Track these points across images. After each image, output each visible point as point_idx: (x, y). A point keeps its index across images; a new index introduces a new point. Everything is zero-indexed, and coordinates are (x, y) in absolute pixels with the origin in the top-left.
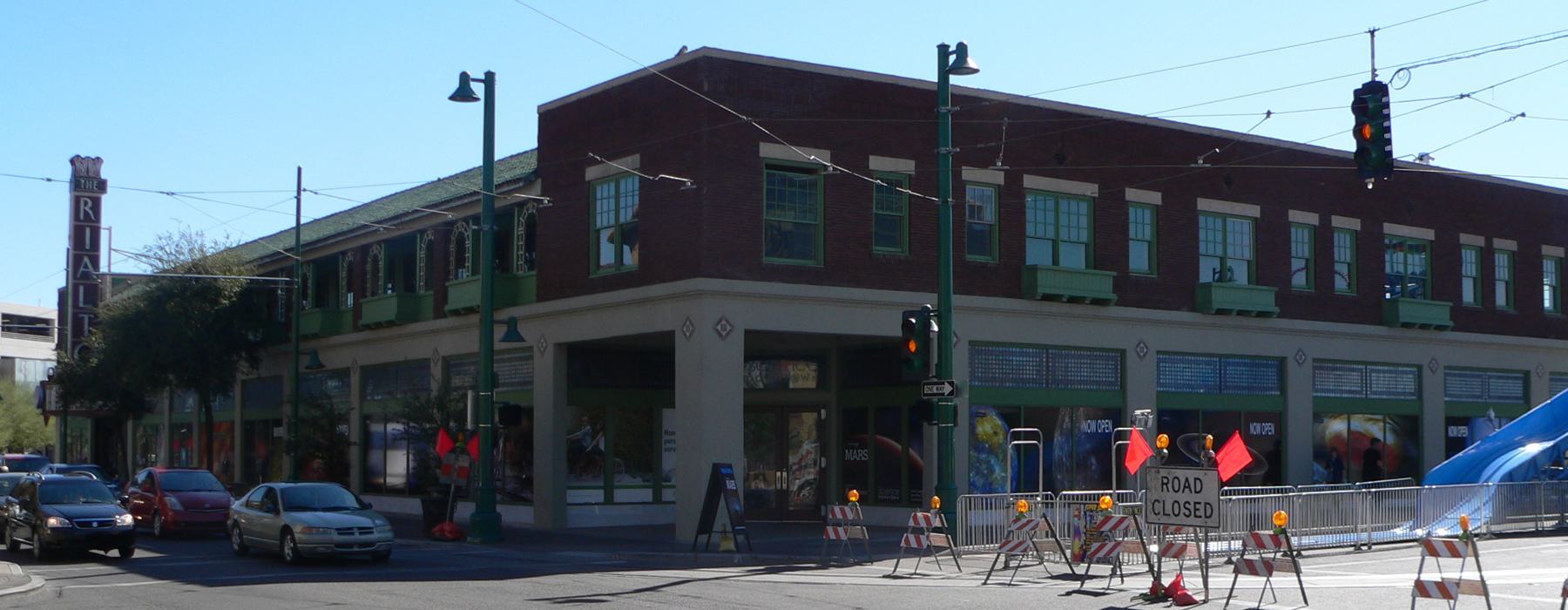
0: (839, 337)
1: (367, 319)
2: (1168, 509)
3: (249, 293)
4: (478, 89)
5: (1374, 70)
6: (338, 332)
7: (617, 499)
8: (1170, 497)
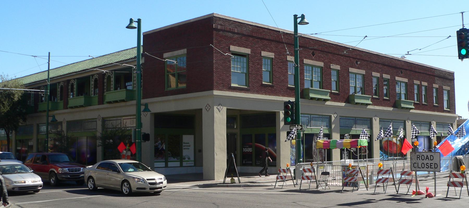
0: (240, 111)
1: (107, 99)
2: (420, 166)
3: (26, 96)
4: (135, 24)
5: (463, 25)
6: (90, 105)
7: (169, 166)
8: (420, 162)
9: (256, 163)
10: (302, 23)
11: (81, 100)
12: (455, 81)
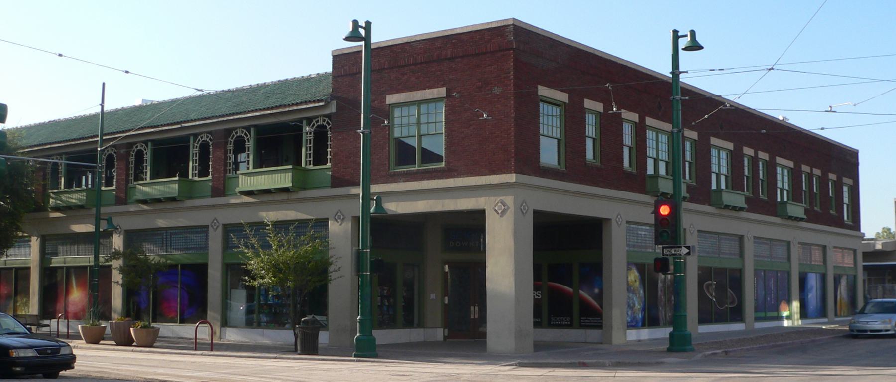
4: (362, 32)
9: (549, 320)
10: (695, 46)
11: (171, 186)
12: (860, 167)
